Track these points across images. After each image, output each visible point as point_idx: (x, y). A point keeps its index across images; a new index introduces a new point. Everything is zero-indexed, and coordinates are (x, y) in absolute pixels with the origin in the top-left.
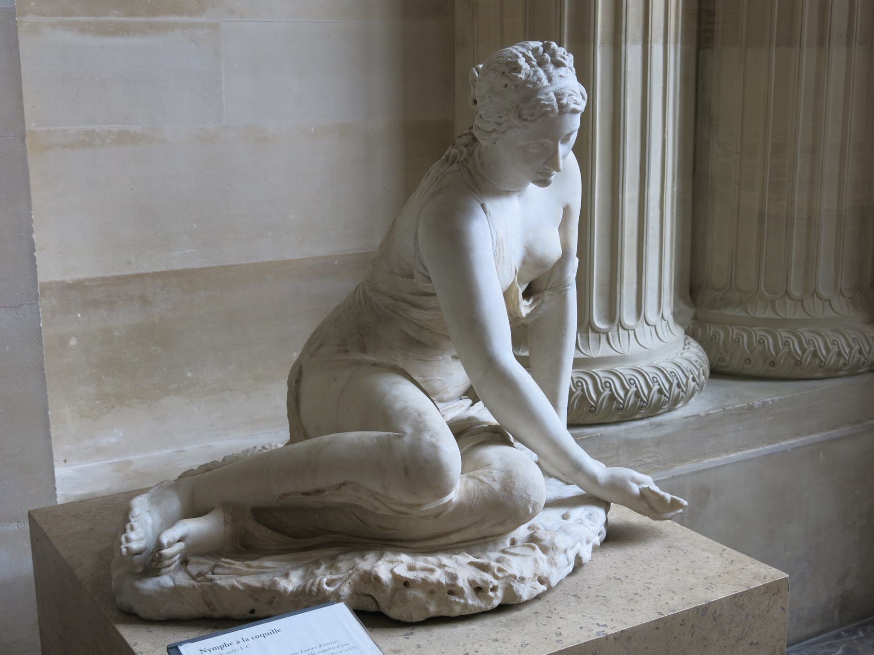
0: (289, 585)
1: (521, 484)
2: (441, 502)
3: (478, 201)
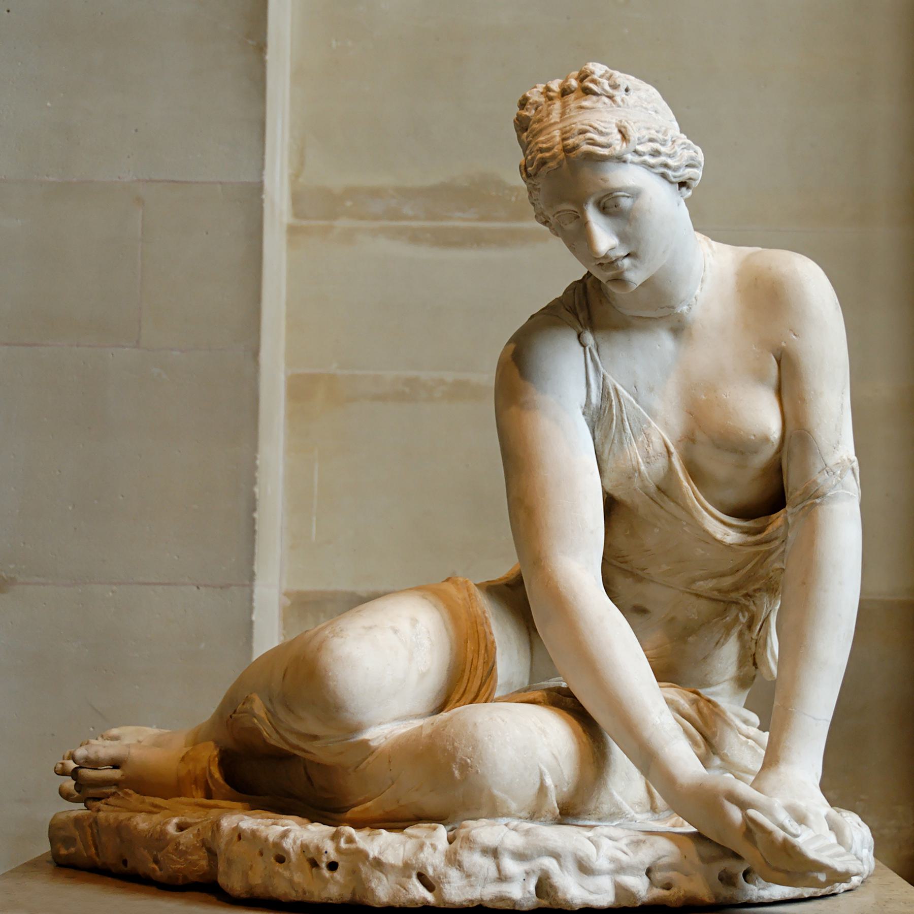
1: (452, 730)
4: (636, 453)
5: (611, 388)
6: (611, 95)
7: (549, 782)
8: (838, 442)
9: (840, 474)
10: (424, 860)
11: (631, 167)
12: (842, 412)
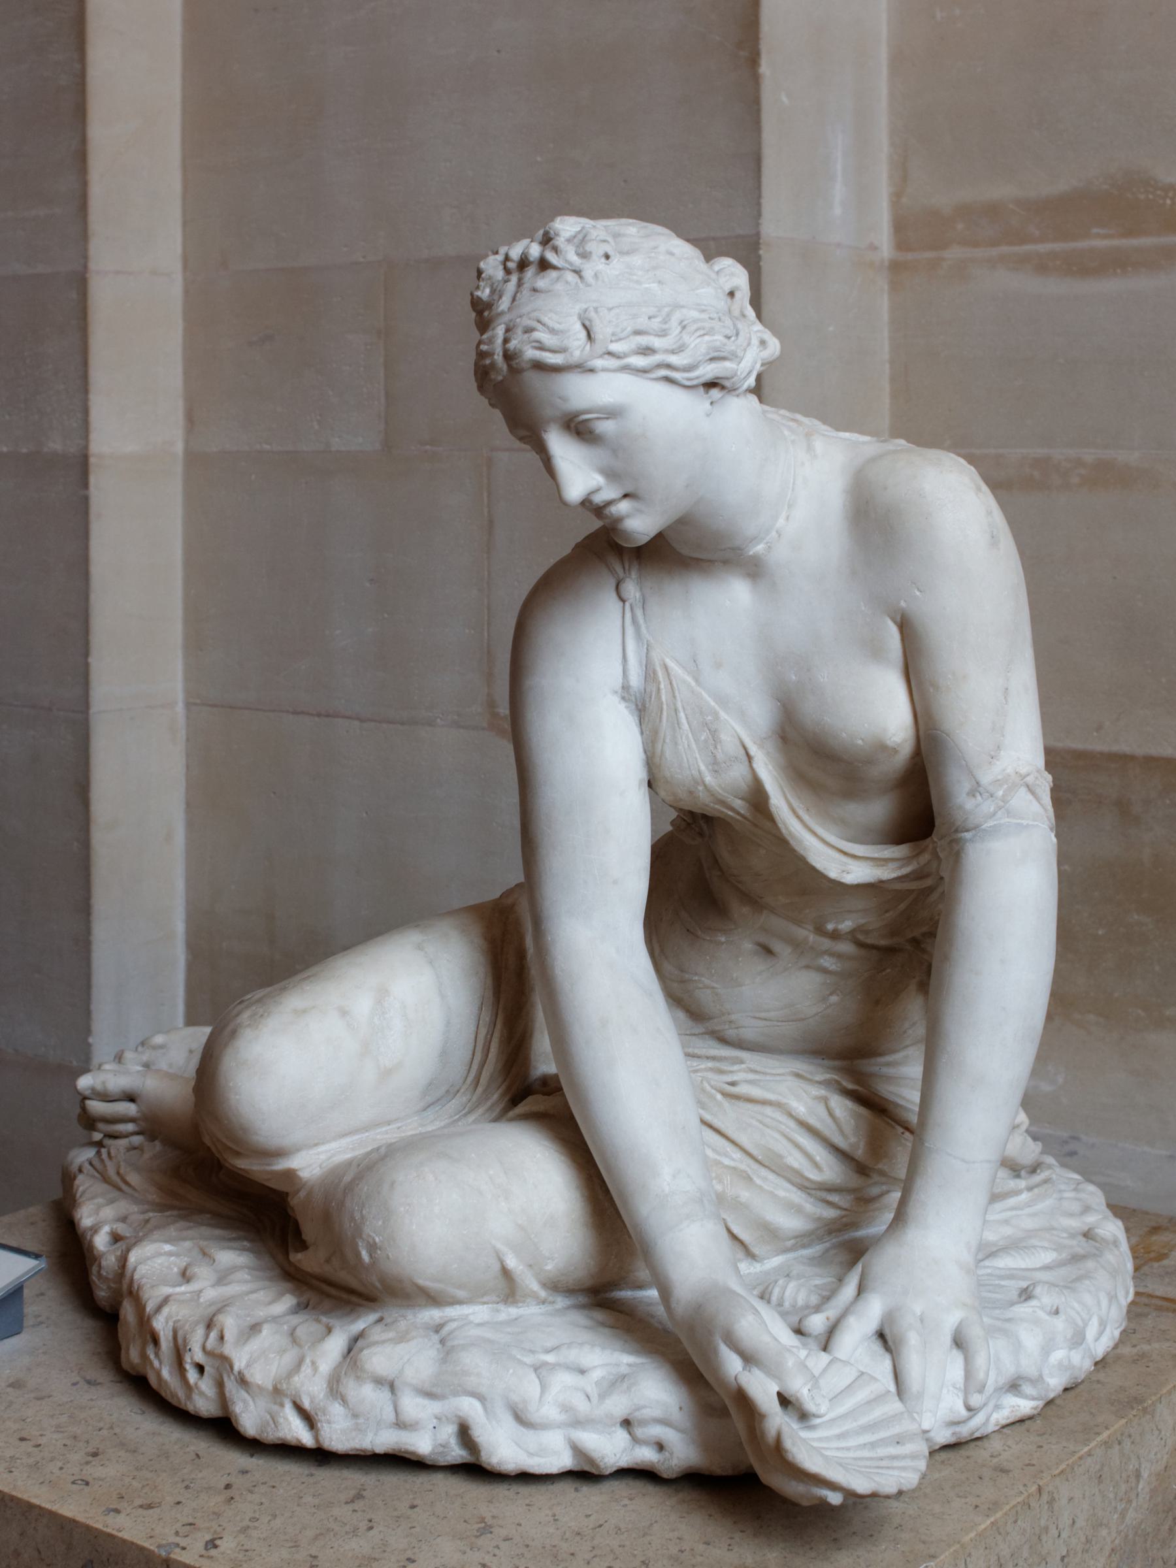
0: (90, 1216)
2: (269, 1165)
3: (612, 571)
4: (696, 758)
5: (657, 664)
6: (577, 269)
7: (512, 1262)
8: (998, 747)
9: (1003, 796)
10: (298, 1385)
11: (603, 376)
12: (1006, 701)
